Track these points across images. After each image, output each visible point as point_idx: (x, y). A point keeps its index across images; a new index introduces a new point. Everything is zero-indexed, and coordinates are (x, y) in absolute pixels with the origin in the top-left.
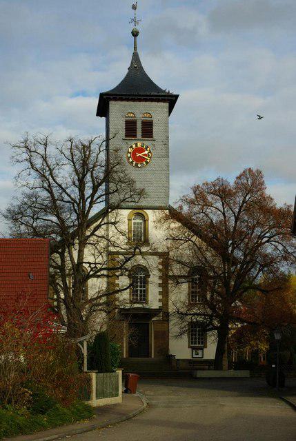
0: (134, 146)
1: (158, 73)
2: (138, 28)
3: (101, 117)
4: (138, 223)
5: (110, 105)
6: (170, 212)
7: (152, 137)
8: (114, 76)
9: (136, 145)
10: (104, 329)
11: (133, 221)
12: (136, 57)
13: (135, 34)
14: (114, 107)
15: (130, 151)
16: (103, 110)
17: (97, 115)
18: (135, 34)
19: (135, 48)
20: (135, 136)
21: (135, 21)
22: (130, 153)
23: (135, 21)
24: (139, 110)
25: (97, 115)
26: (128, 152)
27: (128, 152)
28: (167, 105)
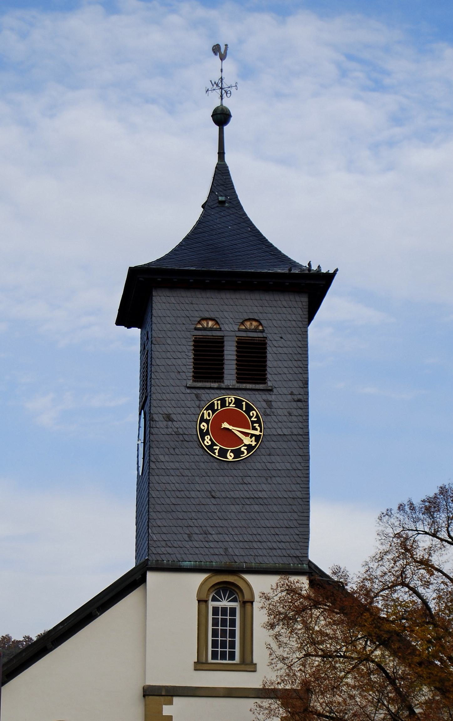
0: (217, 404)
1: (288, 220)
2: (228, 103)
3: (129, 327)
4: (224, 610)
5: (154, 299)
6: (312, 584)
7: (263, 380)
8: (163, 227)
9: (223, 402)
10: (279, 702)
11: (212, 604)
12: (222, 175)
13: (221, 117)
14: (163, 304)
15: (206, 416)
16: (132, 311)
17: (172, 704)
18: (221, 117)
19: (221, 154)
20: (219, 377)
21: (221, 87)
22: (207, 421)
23: (221, 87)
24: (231, 315)
25: (118, 323)
26: (203, 420)
27: (203, 420)
28: (304, 300)
